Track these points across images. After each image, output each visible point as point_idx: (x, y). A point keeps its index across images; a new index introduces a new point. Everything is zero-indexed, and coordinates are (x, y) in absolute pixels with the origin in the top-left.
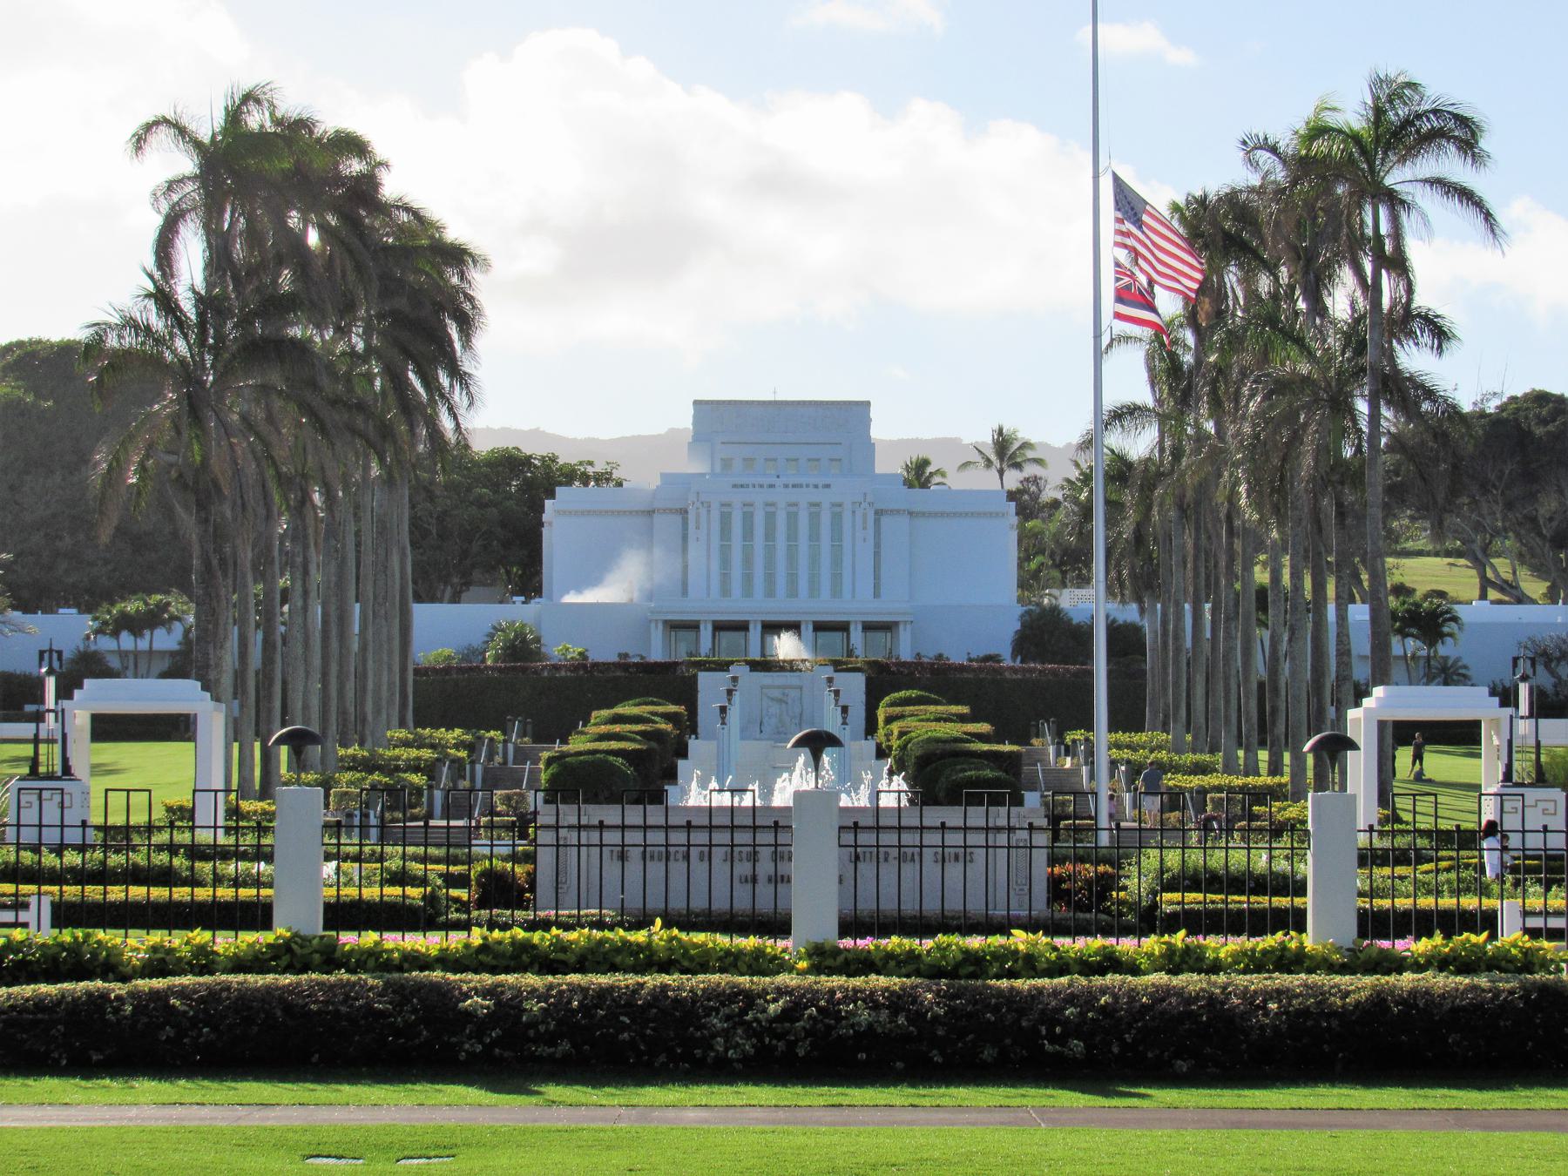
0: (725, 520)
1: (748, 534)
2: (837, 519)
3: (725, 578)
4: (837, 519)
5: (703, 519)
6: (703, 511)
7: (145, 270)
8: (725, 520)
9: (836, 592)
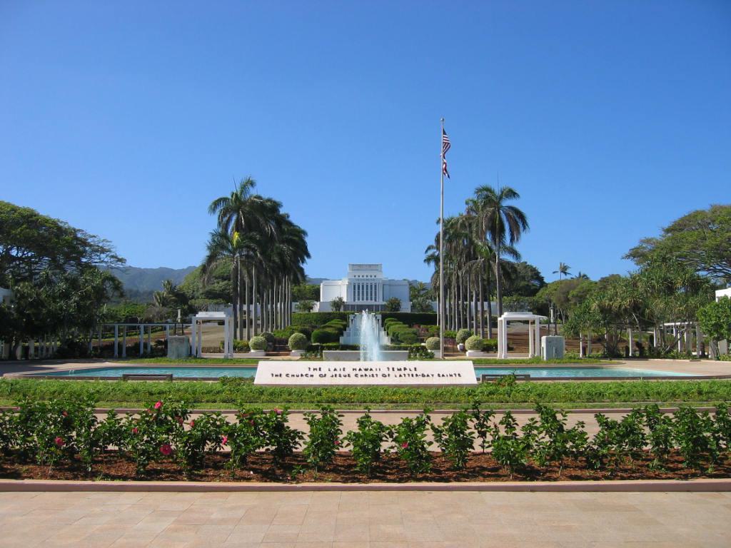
0: (354, 286)
1: (367, 289)
2: (375, 286)
4: (375, 286)
9: (375, 300)
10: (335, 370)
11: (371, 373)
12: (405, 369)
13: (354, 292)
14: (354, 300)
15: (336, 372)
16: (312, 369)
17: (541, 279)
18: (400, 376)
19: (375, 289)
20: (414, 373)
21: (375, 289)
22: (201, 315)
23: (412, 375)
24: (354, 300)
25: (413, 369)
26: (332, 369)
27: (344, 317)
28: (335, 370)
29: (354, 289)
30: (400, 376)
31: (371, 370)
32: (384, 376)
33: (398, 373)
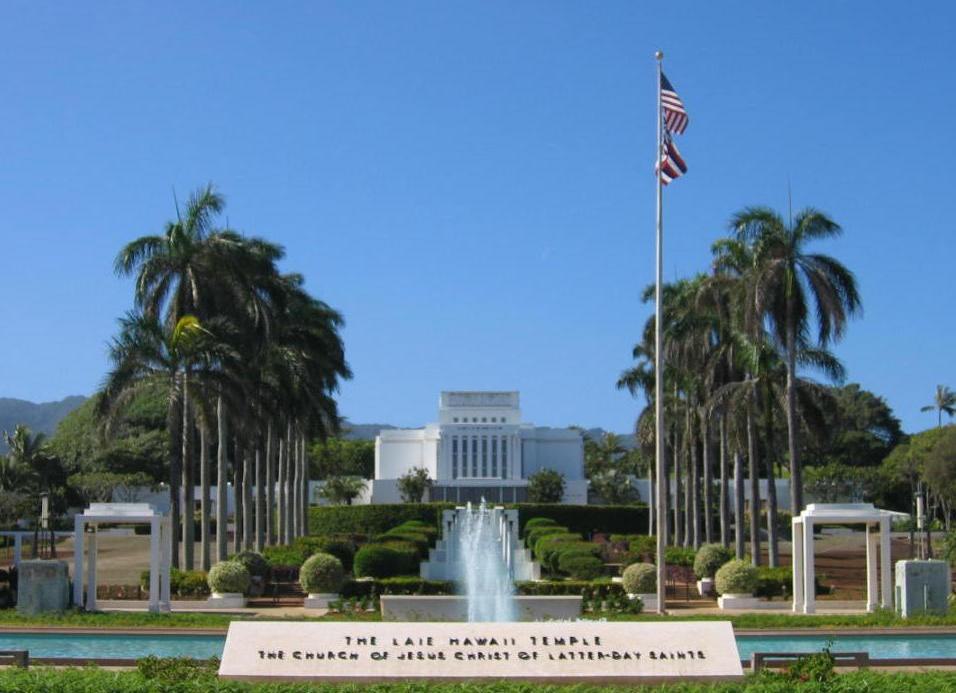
2: (504, 442)
4: (504, 442)
7: (213, 203)
10: (409, 642)
11: (494, 649)
12: (573, 640)
13: (455, 458)
14: (455, 475)
15: (410, 648)
16: (354, 641)
17: (892, 426)
18: (562, 656)
19: (504, 449)
20: (595, 650)
21: (504, 449)
22: (96, 511)
23: (590, 655)
24: (455, 475)
25: (591, 641)
26: (402, 641)
27: (430, 516)
28: (409, 642)
30: (562, 656)
31: (493, 642)
32: (523, 656)
33: (556, 650)
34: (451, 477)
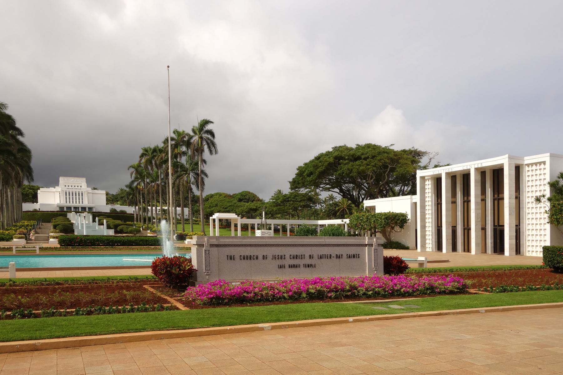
0: (66, 193)
2: (82, 194)
3: (82, 195)
4: (82, 194)
5: (63, 193)
6: (63, 192)
8: (66, 193)
24: (66, 202)
29: (66, 195)
34: (65, 202)
